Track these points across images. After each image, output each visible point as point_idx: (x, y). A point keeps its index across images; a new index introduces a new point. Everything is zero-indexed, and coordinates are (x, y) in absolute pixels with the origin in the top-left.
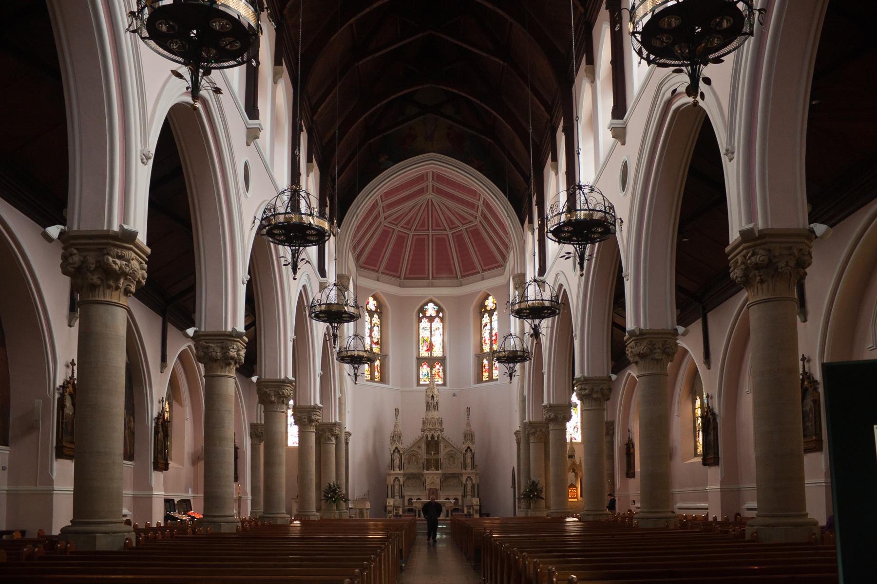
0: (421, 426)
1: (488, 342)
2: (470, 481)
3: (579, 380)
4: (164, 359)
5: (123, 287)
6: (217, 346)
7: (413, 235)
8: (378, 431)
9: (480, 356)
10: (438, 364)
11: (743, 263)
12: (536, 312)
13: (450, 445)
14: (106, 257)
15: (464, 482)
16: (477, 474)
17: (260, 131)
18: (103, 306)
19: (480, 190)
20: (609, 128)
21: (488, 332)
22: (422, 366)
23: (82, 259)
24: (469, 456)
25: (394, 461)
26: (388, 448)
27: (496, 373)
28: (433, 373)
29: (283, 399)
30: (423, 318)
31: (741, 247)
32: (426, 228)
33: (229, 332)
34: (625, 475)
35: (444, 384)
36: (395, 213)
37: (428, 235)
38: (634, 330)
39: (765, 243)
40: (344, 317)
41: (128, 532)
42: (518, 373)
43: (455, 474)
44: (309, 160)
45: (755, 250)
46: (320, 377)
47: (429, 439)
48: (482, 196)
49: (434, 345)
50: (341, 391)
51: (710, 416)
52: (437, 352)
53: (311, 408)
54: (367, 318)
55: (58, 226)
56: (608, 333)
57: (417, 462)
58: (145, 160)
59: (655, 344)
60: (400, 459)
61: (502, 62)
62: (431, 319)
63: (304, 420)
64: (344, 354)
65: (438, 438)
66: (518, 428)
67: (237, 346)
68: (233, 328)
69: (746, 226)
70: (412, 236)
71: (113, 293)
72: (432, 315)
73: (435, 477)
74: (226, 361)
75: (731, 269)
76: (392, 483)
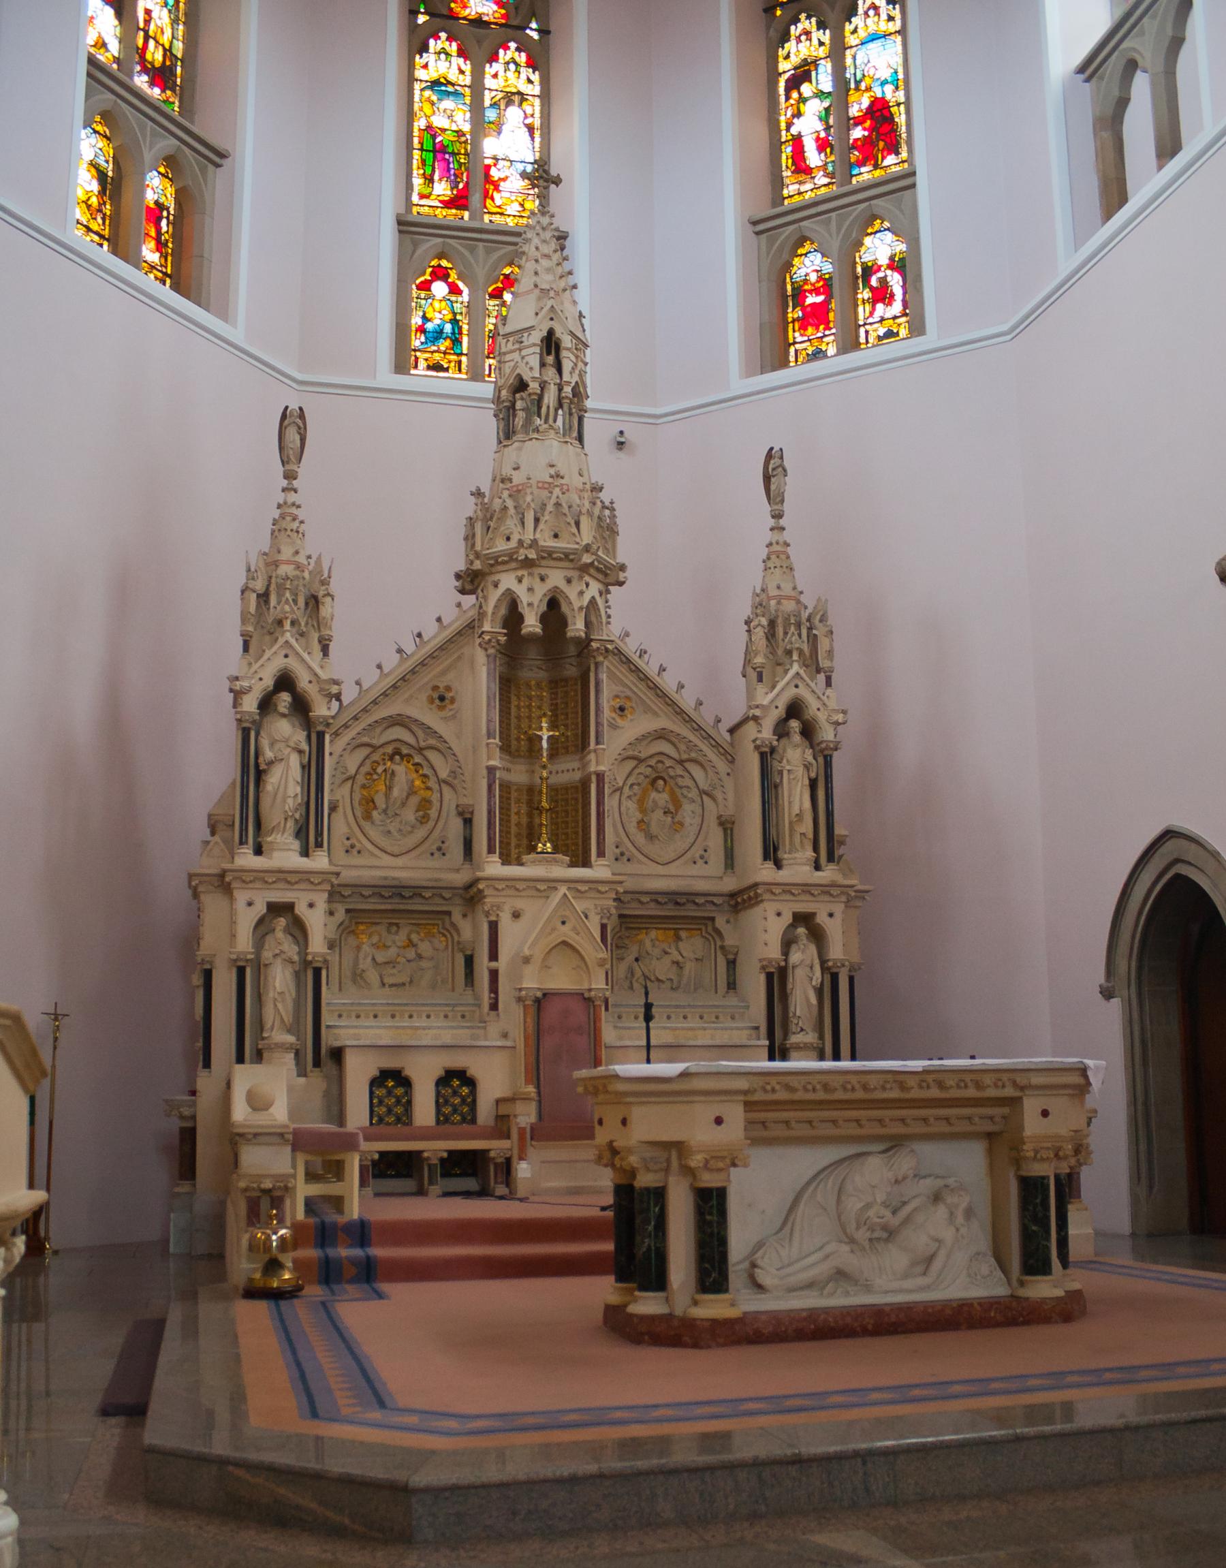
2: (812, 949)
13: (649, 697)
25: (260, 774)
43: (690, 897)
47: (532, 623)
57: (425, 804)
60: (305, 768)
76: (244, 942)
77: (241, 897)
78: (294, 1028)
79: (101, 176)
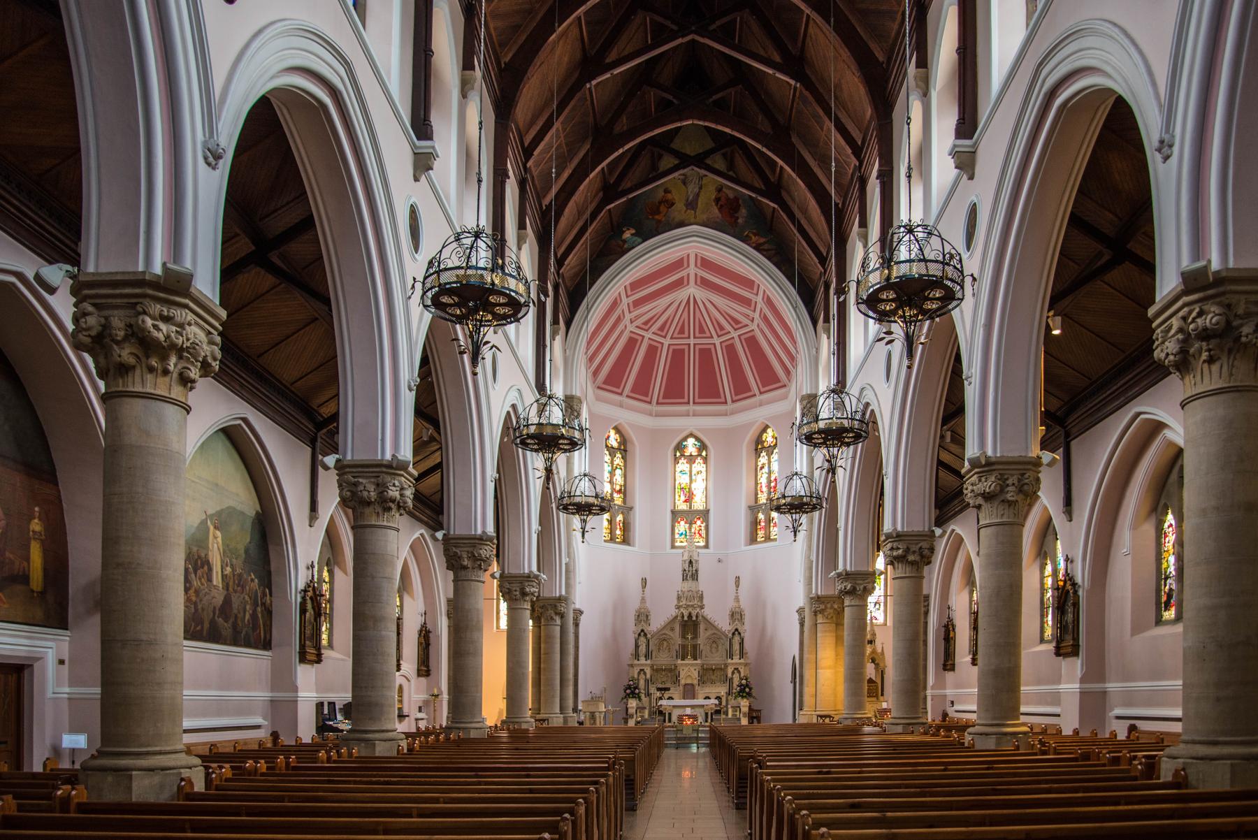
0: (675, 602)
1: (765, 489)
3: (888, 536)
4: (314, 507)
5: (176, 370)
6: (370, 482)
7: (669, 345)
8: (618, 606)
9: (754, 508)
10: (699, 519)
11: (1181, 330)
12: (833, 436)
14: (141, 317)
15: (730, 675)
16: (746, 665)
18: (159, 403)
19: (759, 279)
20: (950, 154)
21: (765, 476)
22: (679, 523)
23: (103, 320)
26: (631, 629)
27: (774, 531)
28: (693, 530)
29: (480, 563)
32: (686, 335)
33: (388, 461)
34: (942, 667)
35: (706, 547)
36: (646, 313)
38: (979, 457)
39: (1223, 294)
40: (562, 444)
41: (190, 768)
42: (804, 527)
44: (521, 226)
47: (686, 618)
48: (762, 288)
50: (569, 555)
51: (1069, 587)
52: (699, 504)
53: (524, 577)
54: (607, 458)
55: (61, 265)
58: (211, 159)
59: (1007, 479)
61: (792, 82)
62: (691, 460)
63: (515, 593)
64: (566, 501)
65: (697, 617)
66: (802, 605)
67: (400, 482)
68: (393, 455)
69: (1186, 263)
71: (158, 380)
72: (693, 454)
73: (692, 669)
74: (384, 504)
75: (1157, 343)
78: (645, 690)
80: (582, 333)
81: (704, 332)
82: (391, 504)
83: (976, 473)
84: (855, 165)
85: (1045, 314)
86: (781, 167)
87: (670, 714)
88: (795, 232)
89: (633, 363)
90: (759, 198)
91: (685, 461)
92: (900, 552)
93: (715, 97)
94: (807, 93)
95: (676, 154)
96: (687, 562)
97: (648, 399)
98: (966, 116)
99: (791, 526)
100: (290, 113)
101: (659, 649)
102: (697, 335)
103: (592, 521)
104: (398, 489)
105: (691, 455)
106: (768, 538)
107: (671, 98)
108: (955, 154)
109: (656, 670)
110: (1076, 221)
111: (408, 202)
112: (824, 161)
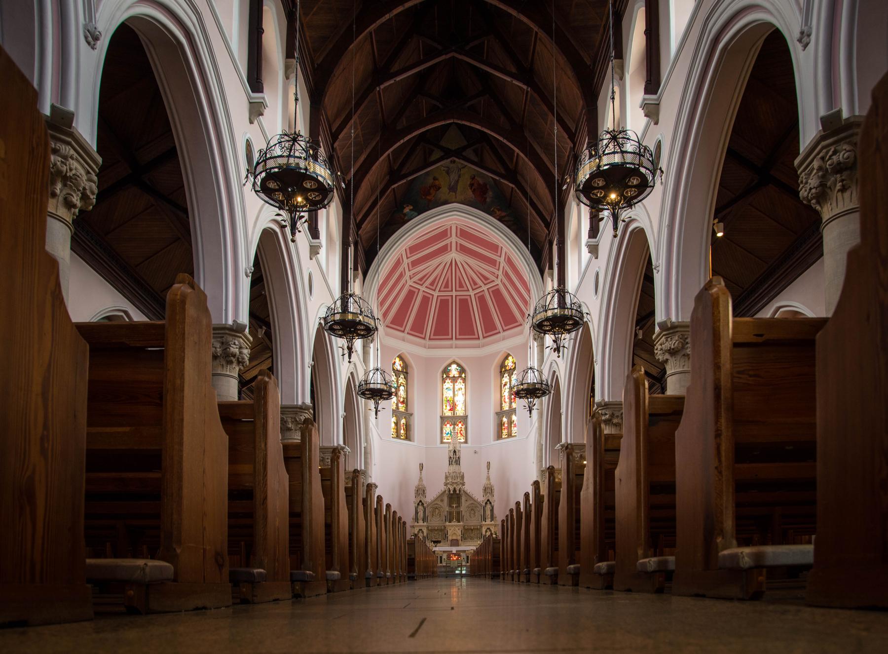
0: (444, 481)
1: (507, 400)
5: (62, 195)
7: (438, 296)
8: (403, 485)
10: (460, 422)
11: (820, 168)
15: (484, 533)
17: (265, 108)
20: (641, 107)
24: (489, 509)
30: (447, 379)
31: (820, 147)
32: (450, 289)
35: (466, 442)
37: (452, 296)
38: (666, 321)
45: (837, 148)
46: (344, 418)
47: (452, 492)
48: (504, 249)
49: (457, 404)
52: (460, 411)
56: (629, 357)
58: (90, 39)
59: (687, 338)
61: (525, 87)
62: (454, 380)
63: (327, 460)
65: (460, 491)
68: (234, 321)
70: (436, 297)
72: (456, 376)
73: (457, 529)
75: (801, 186)
77: (416, 528)
79: (395, 423)
80: (375, 280)
81: (463, 287)
82: (232, 358)
83: (664, 335)
84: (571, 147)
85: (712, 222)
86: (518, 154)
87: (441, 557)
88: (529, 205)
89: (412, 310)
90: (502, 180)
91: (450, 381)
92: (607, 416)
93: (469, 104)
94: (535, 95)
95: (442, 149)
96: (452, 451)
97: (423, 336)
98: (652, 78)
99: (527, 406)
100: (155, 49)
101: (433, 515)
102: (458, 289)
103: (382, 403)
104: (238, 347)
105: (454, 377)
106: (510, 435)
107: (438, 104)
108: (645, 106)
109: (431, 530)
110: (732, 155)
111: (245, 136)
112: (548, 149)
